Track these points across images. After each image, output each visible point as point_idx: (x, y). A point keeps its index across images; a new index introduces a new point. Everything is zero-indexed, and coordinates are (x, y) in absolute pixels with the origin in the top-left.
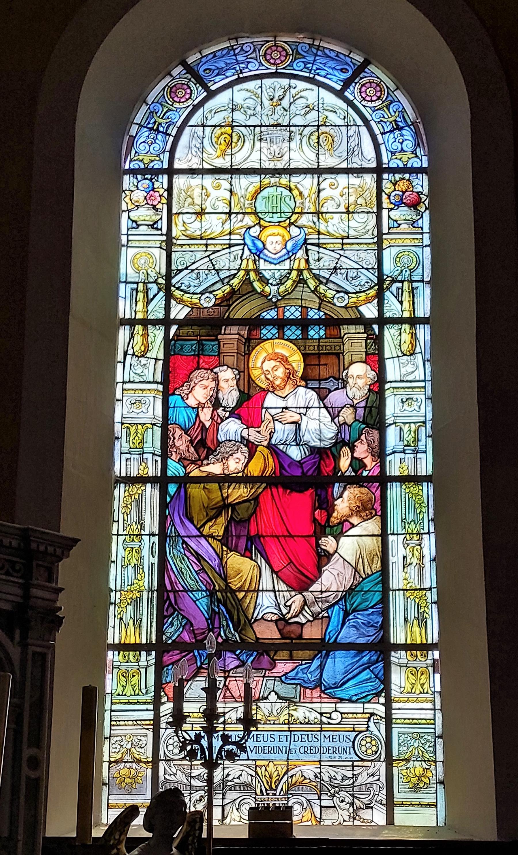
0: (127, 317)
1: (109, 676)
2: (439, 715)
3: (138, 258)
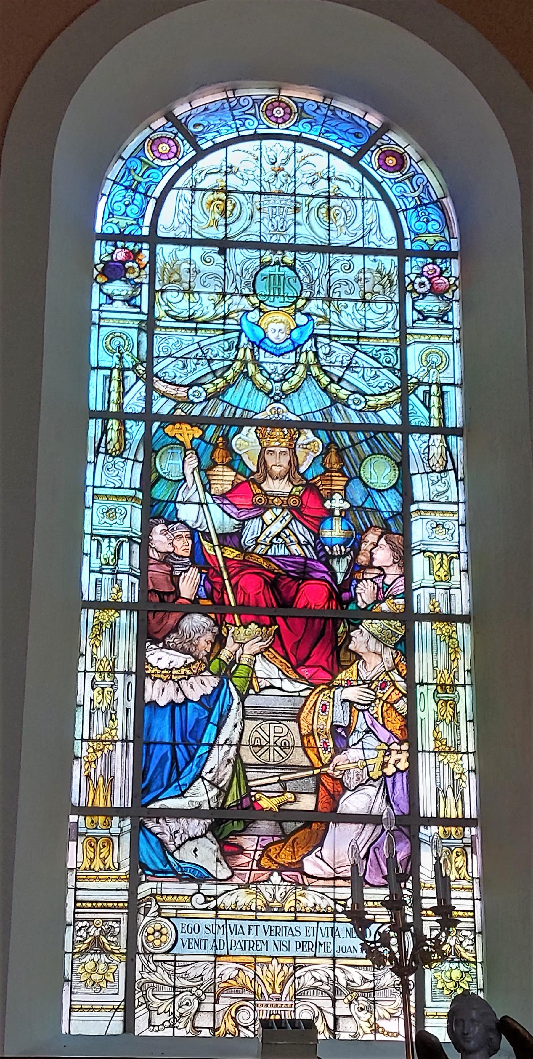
0: (99, 408)
1: (72, 844)
2: (70, 919)
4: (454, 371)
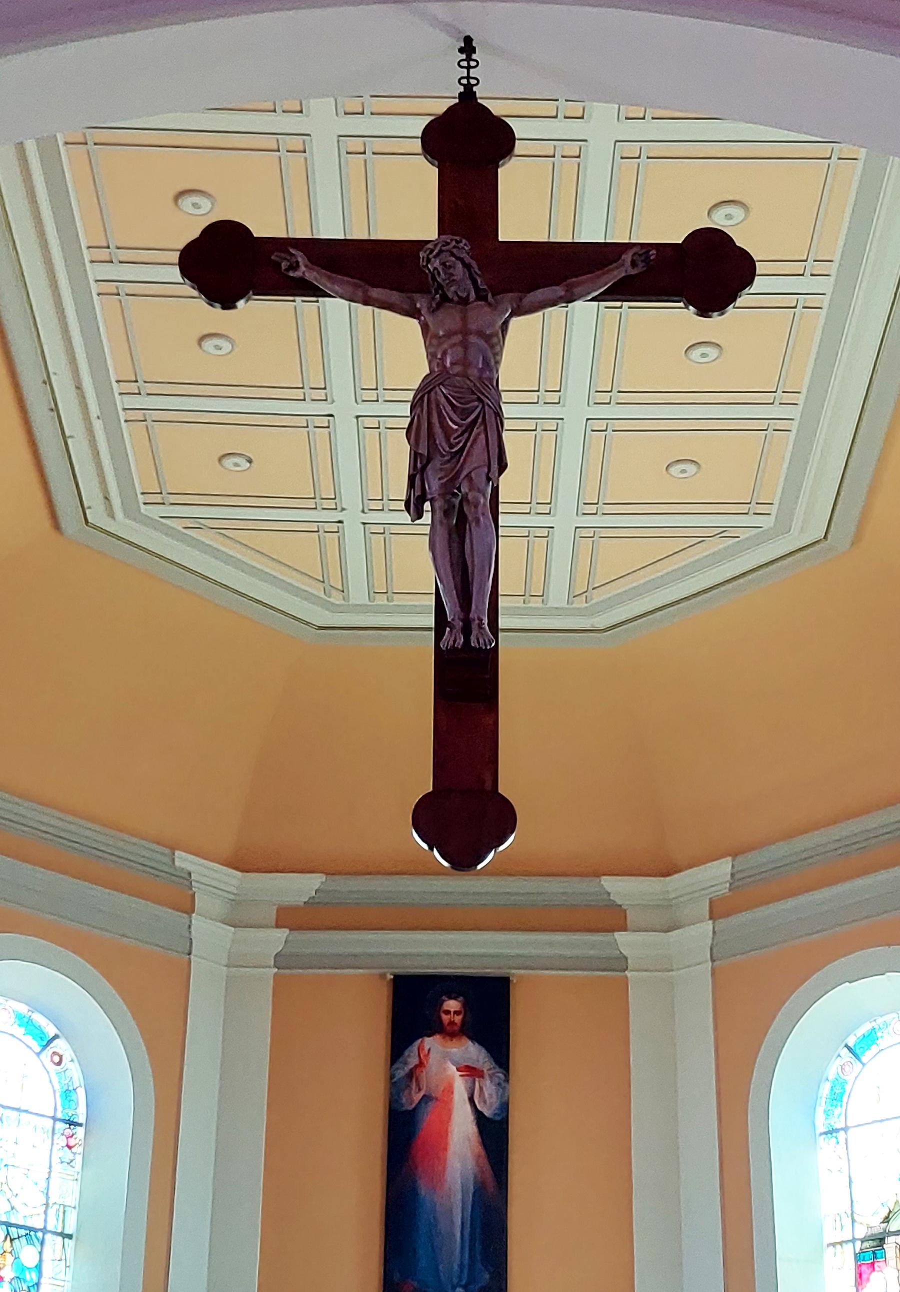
3: (831, 1202)
4: (72, 1199)
